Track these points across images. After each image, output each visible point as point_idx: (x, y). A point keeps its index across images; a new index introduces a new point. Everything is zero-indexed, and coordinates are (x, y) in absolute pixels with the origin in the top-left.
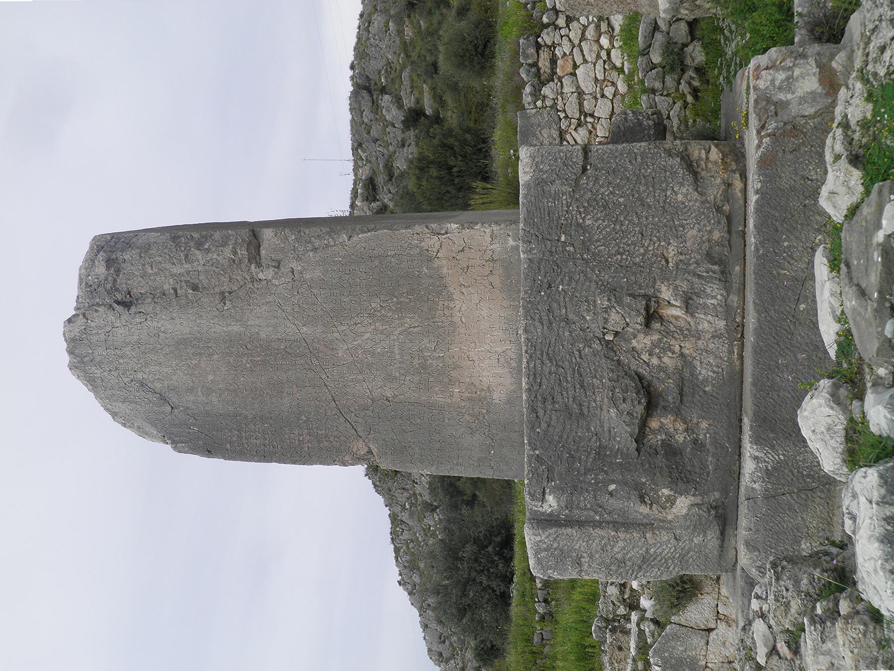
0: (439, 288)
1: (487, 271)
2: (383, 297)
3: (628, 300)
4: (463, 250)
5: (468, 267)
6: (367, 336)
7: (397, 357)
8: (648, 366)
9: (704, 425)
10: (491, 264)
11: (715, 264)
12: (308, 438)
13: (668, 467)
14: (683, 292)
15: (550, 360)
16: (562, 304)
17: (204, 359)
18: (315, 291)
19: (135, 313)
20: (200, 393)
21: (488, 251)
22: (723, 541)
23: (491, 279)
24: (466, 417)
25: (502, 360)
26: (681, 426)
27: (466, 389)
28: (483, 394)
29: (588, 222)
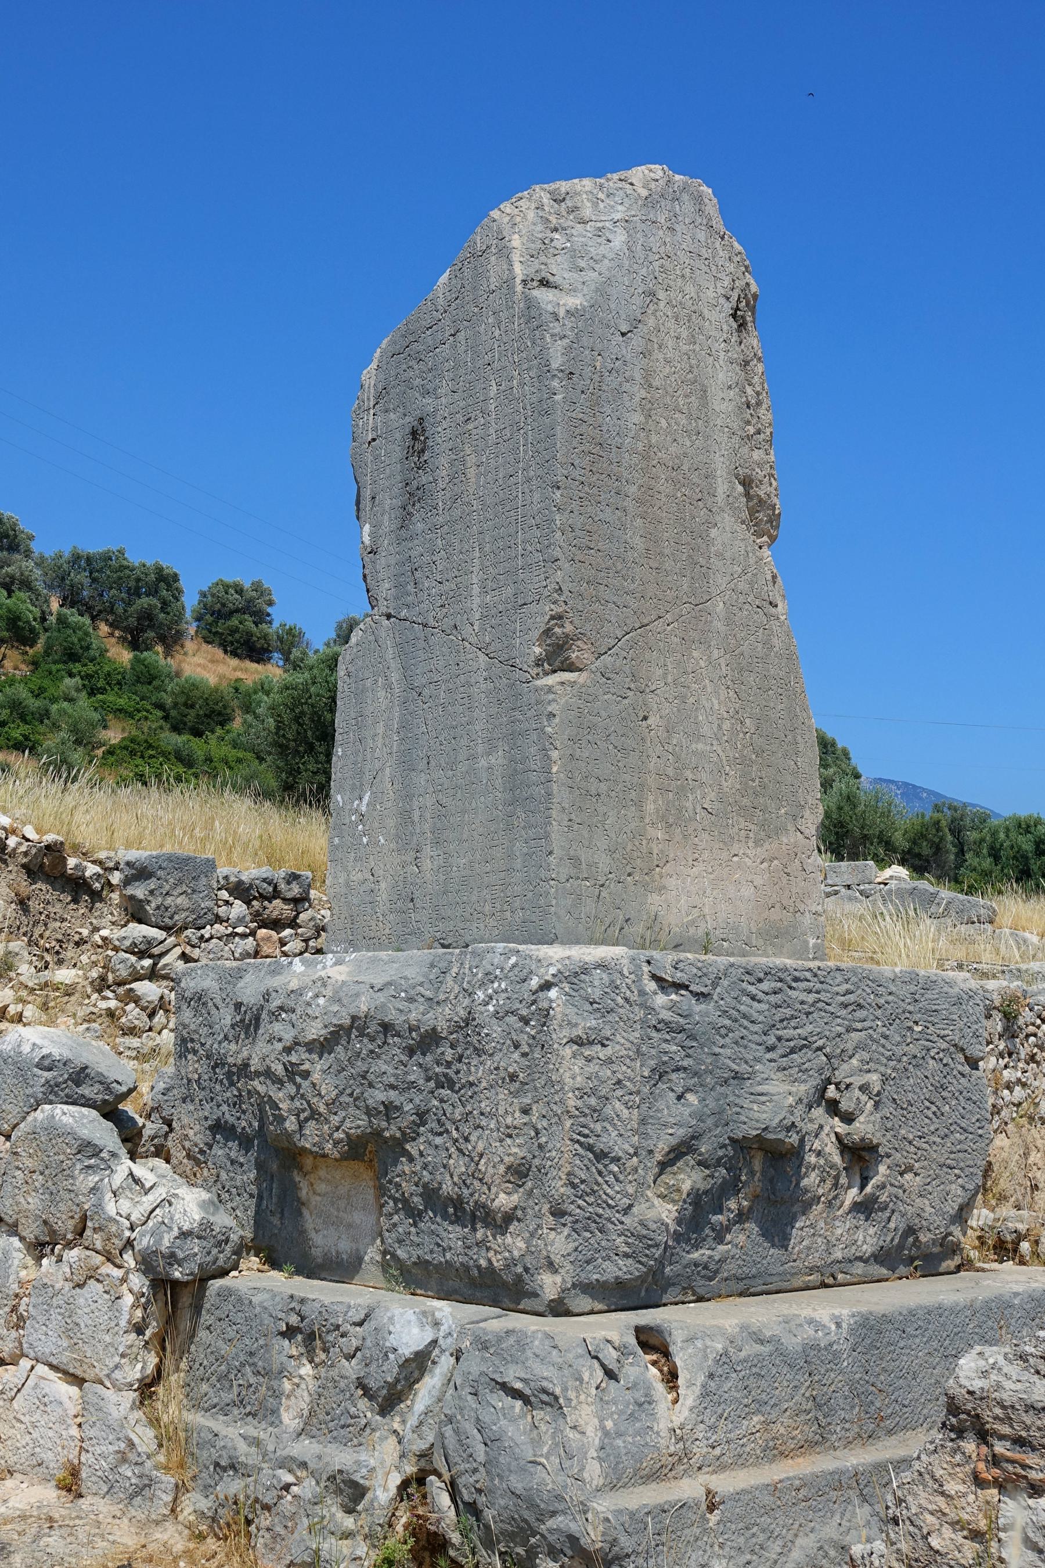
5: (788, 874)
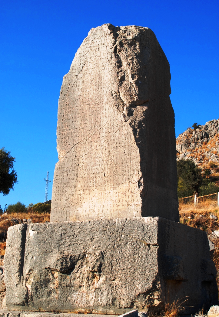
0: (118, 184)
1: (124, 203)
2: (115, 160)
3: (98, 263)
4: (132, 193)
5: (126, 195)
6: (101, 154)
7: (94, 168)
8: (76, 272)
9: (56, 296)
10: (127, 205)
11: (112, 302)
12: (66, 133)
13: (41, 281)
14: (102, 287)
15: (79, 232)
16: (98, 236)
17: (94, 87)
18: (118, 132)
19: (112, 55)
20: (82, 86)
21: (131, 203)
22: (16, 305)
23: (121, 205)
24: (72, 197)
25: (92, 211)
26: (55, 286)
27: (82, 196)
28: (80, 203)
29: (128, 246)
